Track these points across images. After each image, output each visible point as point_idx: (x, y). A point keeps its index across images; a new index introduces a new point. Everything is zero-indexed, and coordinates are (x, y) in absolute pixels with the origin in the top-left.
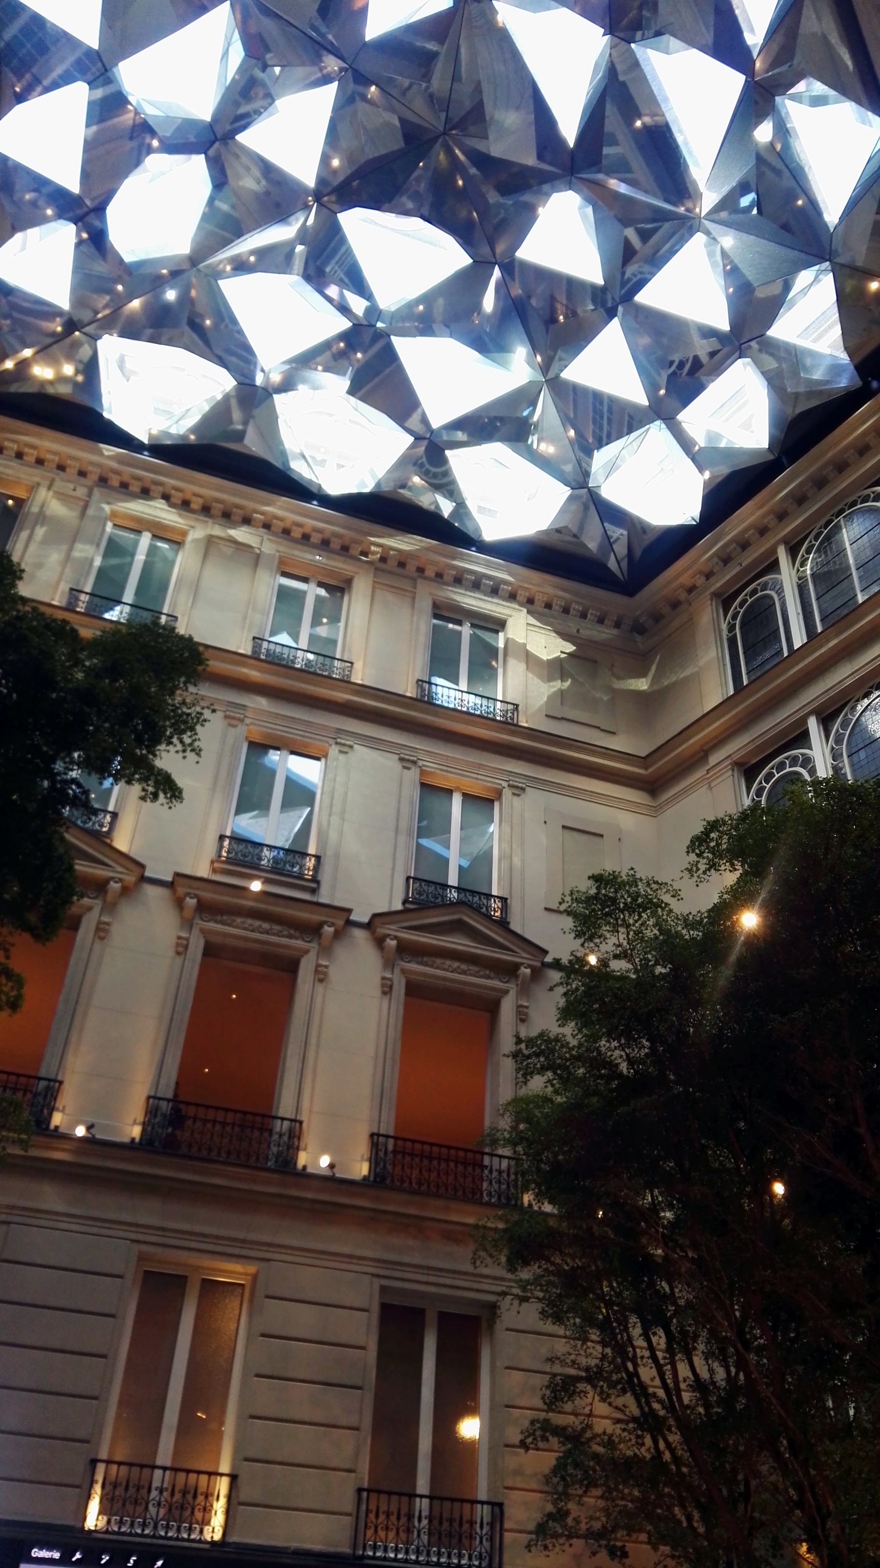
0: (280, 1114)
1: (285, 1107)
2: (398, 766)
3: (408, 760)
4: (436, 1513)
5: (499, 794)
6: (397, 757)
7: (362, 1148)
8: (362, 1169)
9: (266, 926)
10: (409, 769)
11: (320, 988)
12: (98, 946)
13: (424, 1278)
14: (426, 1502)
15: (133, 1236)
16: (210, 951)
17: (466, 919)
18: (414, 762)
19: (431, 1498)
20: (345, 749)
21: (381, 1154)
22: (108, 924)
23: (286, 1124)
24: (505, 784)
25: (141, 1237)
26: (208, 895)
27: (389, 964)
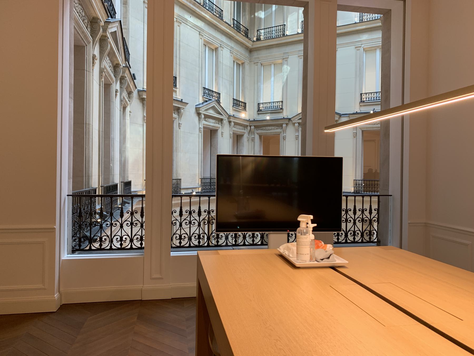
6: (297, 56)
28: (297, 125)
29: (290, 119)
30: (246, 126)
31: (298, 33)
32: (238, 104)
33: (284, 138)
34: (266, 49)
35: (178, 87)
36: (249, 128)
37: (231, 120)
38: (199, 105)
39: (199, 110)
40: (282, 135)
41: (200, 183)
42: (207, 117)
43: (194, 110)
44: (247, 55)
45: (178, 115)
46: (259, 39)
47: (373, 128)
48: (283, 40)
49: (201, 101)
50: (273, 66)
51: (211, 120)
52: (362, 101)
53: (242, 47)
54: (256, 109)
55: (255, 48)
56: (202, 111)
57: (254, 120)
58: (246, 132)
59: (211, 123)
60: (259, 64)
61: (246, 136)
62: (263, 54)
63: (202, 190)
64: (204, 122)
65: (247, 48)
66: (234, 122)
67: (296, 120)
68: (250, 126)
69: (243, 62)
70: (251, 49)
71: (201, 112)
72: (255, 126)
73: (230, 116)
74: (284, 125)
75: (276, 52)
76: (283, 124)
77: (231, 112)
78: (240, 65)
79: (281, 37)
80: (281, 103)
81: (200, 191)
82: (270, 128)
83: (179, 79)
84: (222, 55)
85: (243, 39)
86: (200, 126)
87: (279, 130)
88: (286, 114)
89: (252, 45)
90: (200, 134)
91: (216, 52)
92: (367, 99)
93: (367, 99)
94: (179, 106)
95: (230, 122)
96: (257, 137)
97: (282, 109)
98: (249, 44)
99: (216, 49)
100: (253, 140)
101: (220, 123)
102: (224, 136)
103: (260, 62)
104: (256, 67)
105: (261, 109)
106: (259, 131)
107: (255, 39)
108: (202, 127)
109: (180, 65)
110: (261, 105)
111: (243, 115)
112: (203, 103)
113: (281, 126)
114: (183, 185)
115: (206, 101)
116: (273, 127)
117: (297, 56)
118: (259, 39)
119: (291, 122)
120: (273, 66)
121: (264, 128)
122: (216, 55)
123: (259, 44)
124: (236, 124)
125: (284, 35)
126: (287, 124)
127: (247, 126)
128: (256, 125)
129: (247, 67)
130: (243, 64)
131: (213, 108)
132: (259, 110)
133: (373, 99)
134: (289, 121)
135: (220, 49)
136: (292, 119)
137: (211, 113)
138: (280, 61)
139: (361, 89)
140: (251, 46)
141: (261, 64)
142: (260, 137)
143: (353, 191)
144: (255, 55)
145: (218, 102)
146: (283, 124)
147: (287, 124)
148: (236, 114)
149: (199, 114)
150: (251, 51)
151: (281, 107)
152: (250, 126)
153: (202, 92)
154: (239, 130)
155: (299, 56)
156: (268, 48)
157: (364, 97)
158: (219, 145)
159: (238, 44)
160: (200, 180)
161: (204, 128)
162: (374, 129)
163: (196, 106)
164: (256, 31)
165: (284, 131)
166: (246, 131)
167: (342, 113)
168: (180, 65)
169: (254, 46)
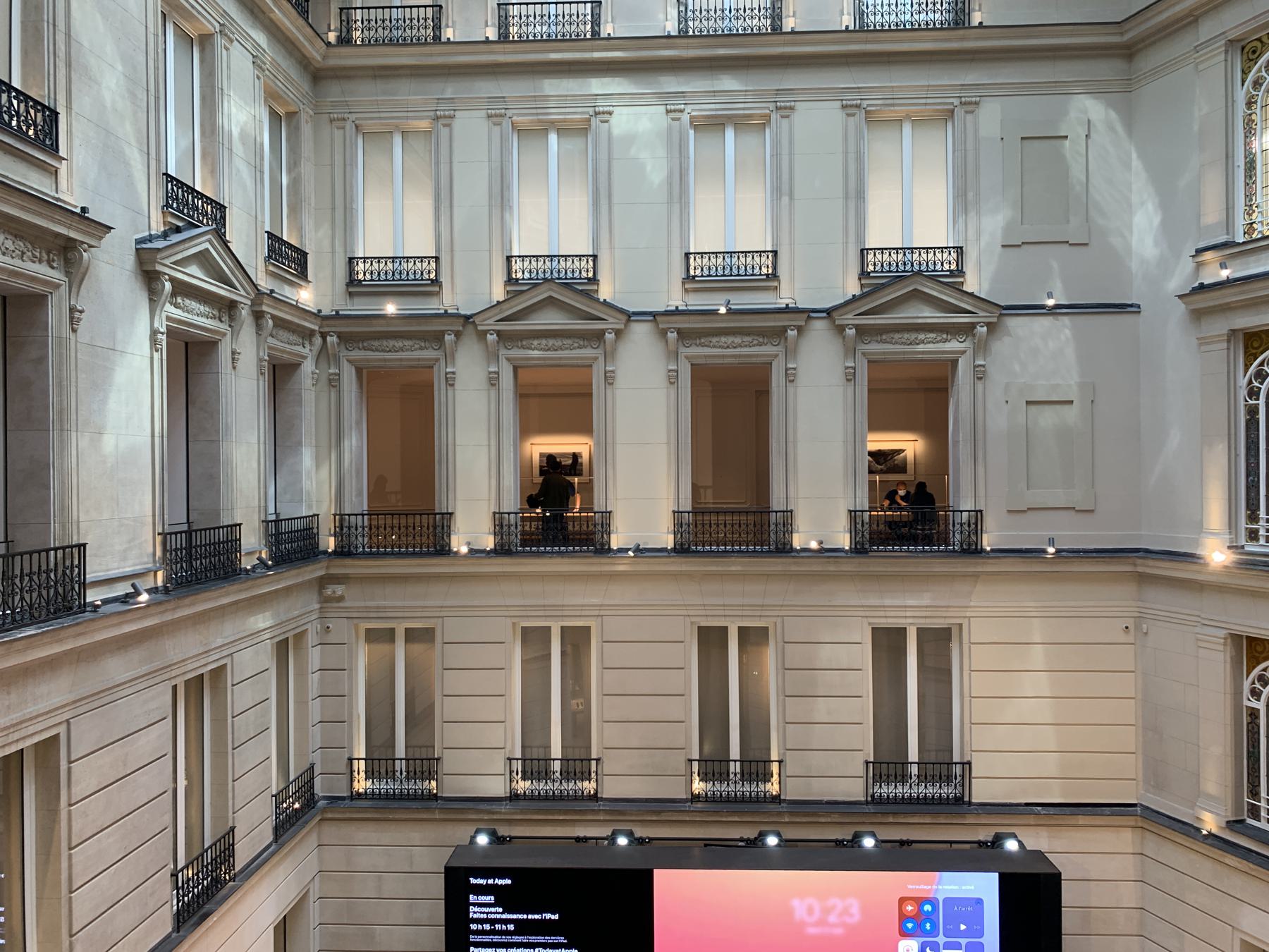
0: (775, 509)
1: (777, 502)
2: (839, 115)
3: (851, 106)
4: (411, 769)
5: (767, 118)
6: (483, 113)
7: (843, 522)
8: (845, 541)
9: (738, 340)
10: (853, 115)
11: (980, 385)
12: (791, 390)
13: (924, 614)
14: (362, 762)
15: (685, 613)
16: (701, 373)
17: (919, 288)
18: (858, 106)
19: (407, 760)
20: (970, 108)
21: (859, 526)
22: (453, 373)
23: (512, 516)
24: (956, 101)
25: (867, 614)
26: (684, 323)
27: (850, 351)
28: (491, 338)
29: (467, 318)
30: (308, 335)
31: (487, 41)
32: (289, 258)
33: (450, 381)
34: (375, 77)
35: (62, 153)
36: (318, 341)
37: (265, 308)
38: (150, 238)
39: (154, 262)
40: (440, 371)
41: (159, 553)
42: (183, 290)
43: (130, 260)
44: (306, 86)
45: (67, 274)
46: (345, 40)
47: (724, 356)
48: (436, 57)
49: (157, 227)
50: (397, 139)
51: (194, 305)
52: (689, 278)
53: (290, 54)
54: (679, 273)
55: (333, 69)
56: (165, 267)
57: (337, 316)
58: (307, 354)
59: (198, 317)
60: (349, 126)
61: (308, 367)
62: (365, 94)
63: (168, 579)
64: (170, 309)
65: (304, 63)
66: (273, 317)
67: (491, 321)
68: (324, 336)
69: (292, 109)
70: (318, 70)
71: (159, 268)
72: (340, 336)
73: (259, 293)
74: (449, 338)
75: (411, 94)
76: (443, 333)
77: (264, 283)
78: (282, 119)
79: (426, 43)
80: (433, 265)
81: (160, 583)
82: (399, 344)
83: (69, 125)
84: (229, 67)
85: (297, 28)
86: (156, 325)
87: (429, 354)
88: (452, 299)
89: (324, 58)
90: (156, 355)
91: (202, 51)
92: (706, 272)
93: (706, 272)
94: (73, 234)
95: (258, 316)
96: (348, 374)
97: (436, 282)
98: (315, 52)
99: (205, 40)
100: (334, 382)
101: (225, 318)
102: (239, 365)
103: (353, 117)
104: (338, 134)
105: (361, 277)
106: (357, 354)
107: (332, 37)
108: (163, 330)
109: (69, 65)
110: (361, 265)
111: (305, 296)
112: (165, 235)
113: (438, 338)
114: (94, 571)
115: (178, 230)
116: (408, 343)
117: (483, 113)
118: (345, 40)
119: (470, 328)
120: (397, 139)
121: (376, 343)
122: (202, 61)
123: (347, 58)
124: (280, 323)
125: (437, 39)
126: (458, 335)
127: (312, 333)
128: (343, 332)
129: (306, 129)
130: (291, 115)
131: (202, 258)
132: (352, 281)
133: (411, 277)
134: (464, 326)
135: (219, 41)
136: (477, 320)
137: (195, 275)
138: (424, 125)
139: (685, 238)
140: (319, 58)
141: (357, 127)
142: (359, 371)
143: (670, 545)
144: (334, 92)
145: (220, 235)
146: (443, 333)
147: (458, 335)
148: (287, 292)
149: (149, 278)
150: (317, 76)
151: (433, 276)
152: (324, 336)
153: (162, 194)
154: (287, 346)
155: (489, 116)
156: (381, 77)
157: (517, 265)
158: (223, 400)
159: (279, 41)
160: (159, 539)
161: (171, 333)
162: (727, 361)
163: (138, 242)
164: (334, 10)
165: (450, 357)
166: (306, 351)
167: (632, 310)
168: (69, 65)
169: (332, 62)
